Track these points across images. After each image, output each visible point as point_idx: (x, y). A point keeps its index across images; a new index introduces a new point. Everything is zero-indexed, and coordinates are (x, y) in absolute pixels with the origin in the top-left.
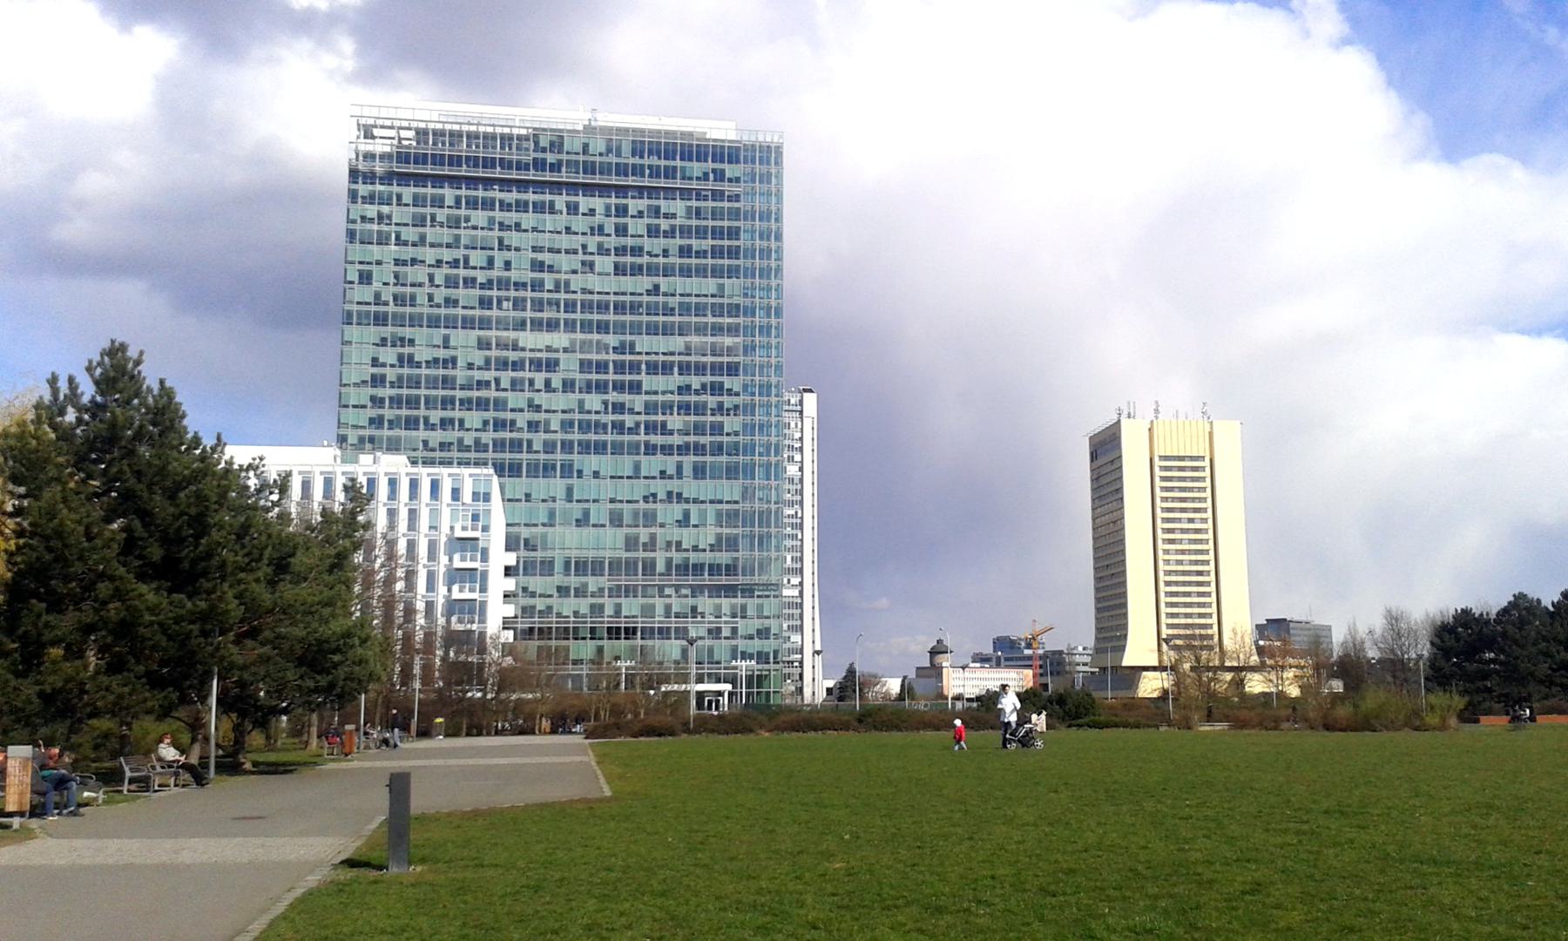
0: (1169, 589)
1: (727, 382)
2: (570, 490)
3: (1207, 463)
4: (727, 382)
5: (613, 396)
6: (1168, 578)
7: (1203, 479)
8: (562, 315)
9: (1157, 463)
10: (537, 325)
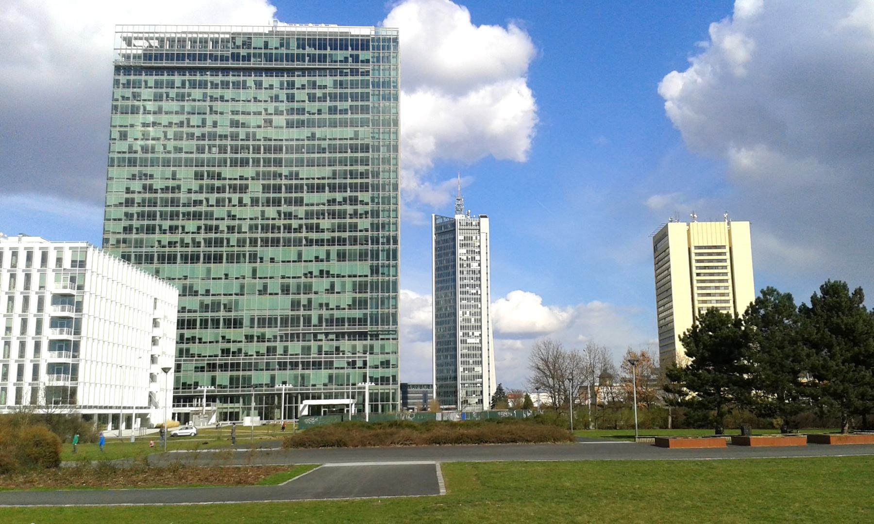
3: (727, 250)
4: (361, 196)
5: (284, 208)
6: (699, 271)
8: (251, 156)
9: (693, 251)
10: (234, 163)
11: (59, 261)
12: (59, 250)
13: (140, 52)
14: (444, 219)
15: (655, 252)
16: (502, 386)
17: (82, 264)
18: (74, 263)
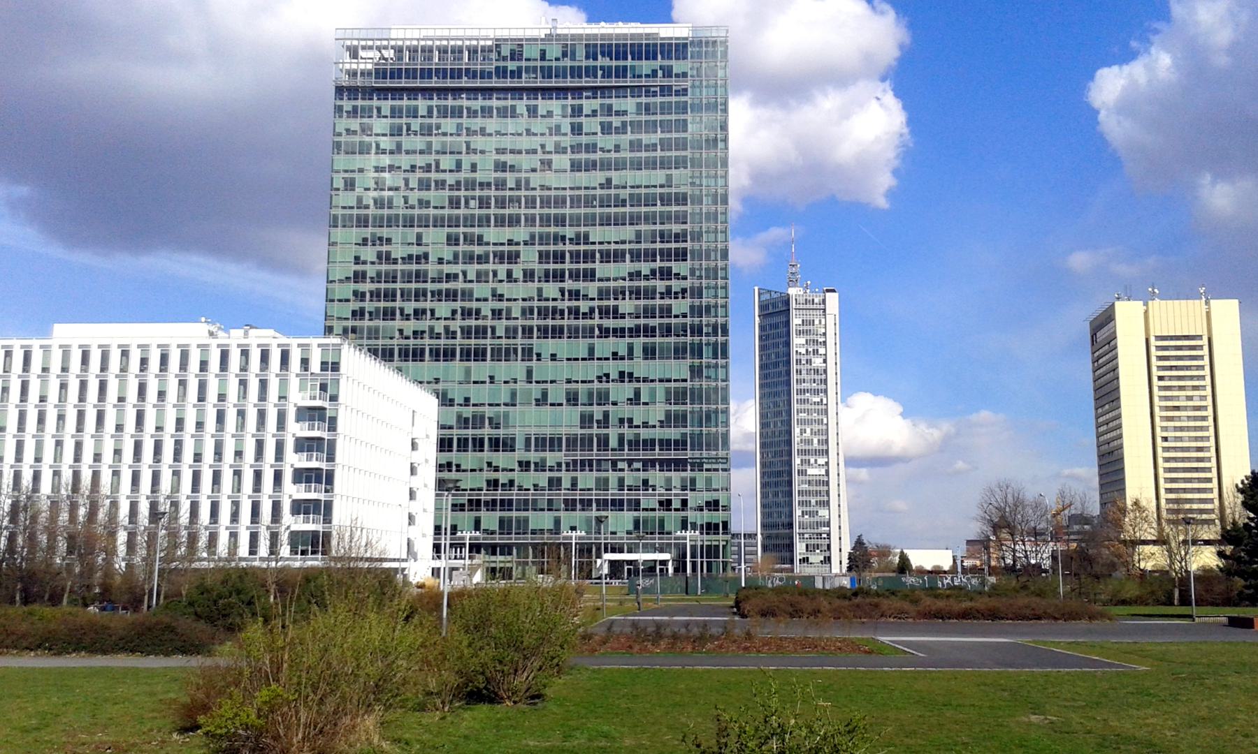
0: (1162, 383)
1: (676, 267)
2: (529, 372)
3: (1205, 342)
4: (676, 267)
5: (569, 284)
7: (1201, 358)
8: (523, 211)
9: (1153, 342)
11: (305, 362)
12: (305, 348)
13: (370, 66)
14: (773, 293)
15: (1093, 344)
16: (863, 538)
17: (336, 367)
18: (324, 366)
